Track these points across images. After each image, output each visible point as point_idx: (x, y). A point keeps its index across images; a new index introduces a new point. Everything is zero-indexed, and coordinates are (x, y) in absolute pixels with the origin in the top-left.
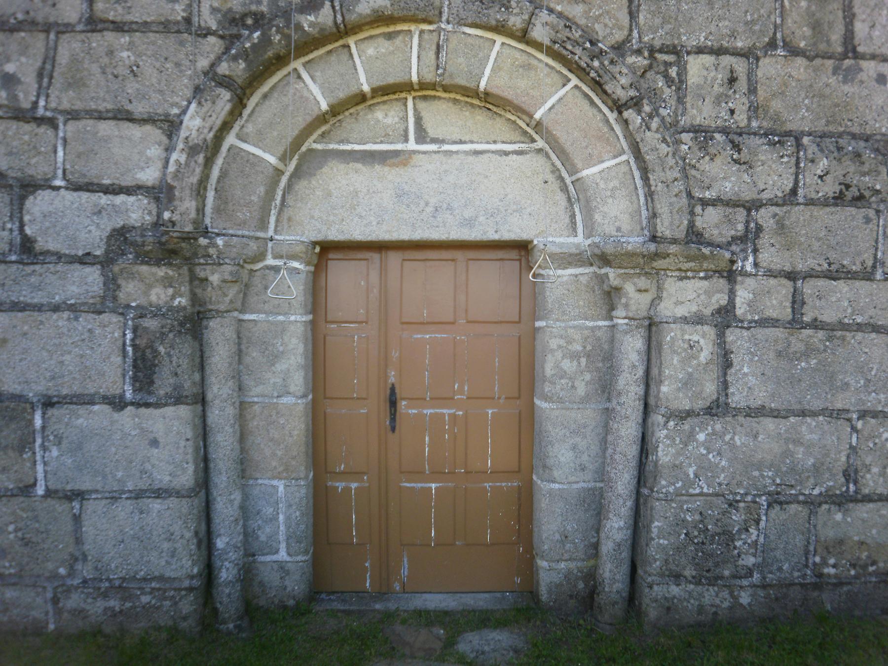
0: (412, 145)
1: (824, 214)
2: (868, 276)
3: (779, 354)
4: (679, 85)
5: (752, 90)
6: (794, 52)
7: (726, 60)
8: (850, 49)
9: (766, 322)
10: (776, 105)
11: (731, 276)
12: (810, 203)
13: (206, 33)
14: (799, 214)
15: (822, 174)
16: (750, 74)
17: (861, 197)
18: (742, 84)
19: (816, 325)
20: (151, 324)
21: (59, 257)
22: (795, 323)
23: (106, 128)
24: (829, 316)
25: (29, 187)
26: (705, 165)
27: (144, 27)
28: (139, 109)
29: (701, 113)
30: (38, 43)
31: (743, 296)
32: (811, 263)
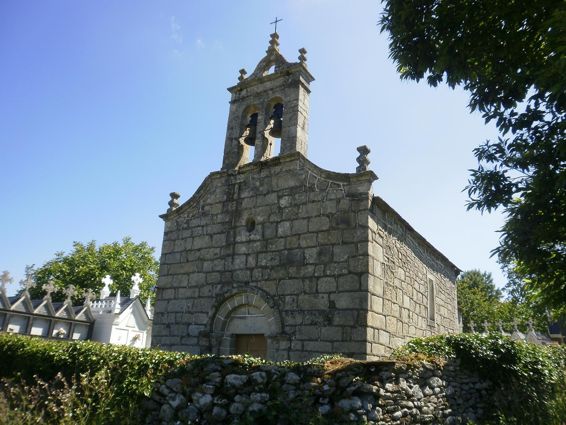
0: (247, 315)
1: (308, 327)
2: (317, 340)
3: (299, 357)
4: (284, 302)
5: (297, 302)
6: (305, 293)
7: (293, 296)
8: (317, 292)
9: (297, 350)
10: (301, 305)
11: (291, 341)
12: (305, 325)
13: (213, 298)
14: (303, 327)
15: (308, 319)
16: (297, 299)
17: (316, 323)
18: (295, 301)
19: (306, 351)
20: (203, 348)
21: (192, 336)
22: (302, 351)
23: (200, 314)
24: (309, 349)
25: (190, 324)
26: (287, 318)
27: (205, 297)
28: (204, 311)
29: (288, 307)
30: (192, 300)
31: (293, 344)
32: (305, 338)
